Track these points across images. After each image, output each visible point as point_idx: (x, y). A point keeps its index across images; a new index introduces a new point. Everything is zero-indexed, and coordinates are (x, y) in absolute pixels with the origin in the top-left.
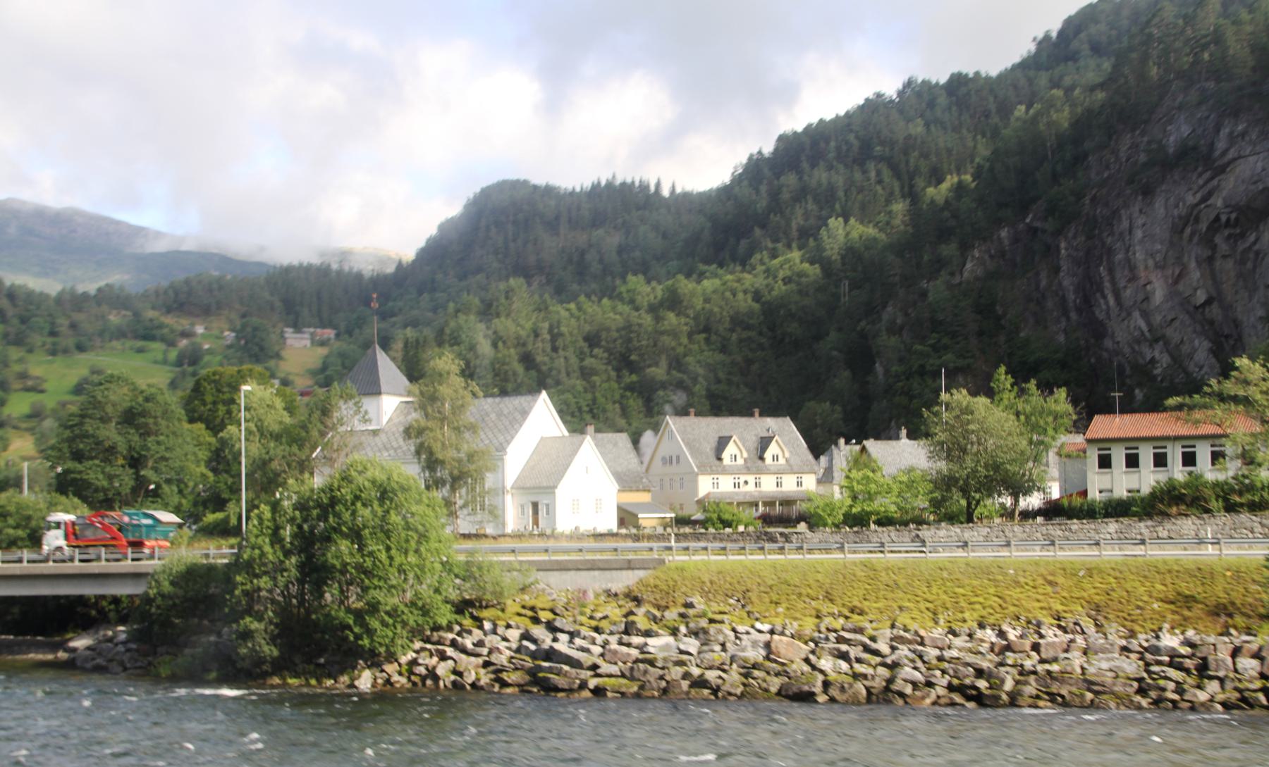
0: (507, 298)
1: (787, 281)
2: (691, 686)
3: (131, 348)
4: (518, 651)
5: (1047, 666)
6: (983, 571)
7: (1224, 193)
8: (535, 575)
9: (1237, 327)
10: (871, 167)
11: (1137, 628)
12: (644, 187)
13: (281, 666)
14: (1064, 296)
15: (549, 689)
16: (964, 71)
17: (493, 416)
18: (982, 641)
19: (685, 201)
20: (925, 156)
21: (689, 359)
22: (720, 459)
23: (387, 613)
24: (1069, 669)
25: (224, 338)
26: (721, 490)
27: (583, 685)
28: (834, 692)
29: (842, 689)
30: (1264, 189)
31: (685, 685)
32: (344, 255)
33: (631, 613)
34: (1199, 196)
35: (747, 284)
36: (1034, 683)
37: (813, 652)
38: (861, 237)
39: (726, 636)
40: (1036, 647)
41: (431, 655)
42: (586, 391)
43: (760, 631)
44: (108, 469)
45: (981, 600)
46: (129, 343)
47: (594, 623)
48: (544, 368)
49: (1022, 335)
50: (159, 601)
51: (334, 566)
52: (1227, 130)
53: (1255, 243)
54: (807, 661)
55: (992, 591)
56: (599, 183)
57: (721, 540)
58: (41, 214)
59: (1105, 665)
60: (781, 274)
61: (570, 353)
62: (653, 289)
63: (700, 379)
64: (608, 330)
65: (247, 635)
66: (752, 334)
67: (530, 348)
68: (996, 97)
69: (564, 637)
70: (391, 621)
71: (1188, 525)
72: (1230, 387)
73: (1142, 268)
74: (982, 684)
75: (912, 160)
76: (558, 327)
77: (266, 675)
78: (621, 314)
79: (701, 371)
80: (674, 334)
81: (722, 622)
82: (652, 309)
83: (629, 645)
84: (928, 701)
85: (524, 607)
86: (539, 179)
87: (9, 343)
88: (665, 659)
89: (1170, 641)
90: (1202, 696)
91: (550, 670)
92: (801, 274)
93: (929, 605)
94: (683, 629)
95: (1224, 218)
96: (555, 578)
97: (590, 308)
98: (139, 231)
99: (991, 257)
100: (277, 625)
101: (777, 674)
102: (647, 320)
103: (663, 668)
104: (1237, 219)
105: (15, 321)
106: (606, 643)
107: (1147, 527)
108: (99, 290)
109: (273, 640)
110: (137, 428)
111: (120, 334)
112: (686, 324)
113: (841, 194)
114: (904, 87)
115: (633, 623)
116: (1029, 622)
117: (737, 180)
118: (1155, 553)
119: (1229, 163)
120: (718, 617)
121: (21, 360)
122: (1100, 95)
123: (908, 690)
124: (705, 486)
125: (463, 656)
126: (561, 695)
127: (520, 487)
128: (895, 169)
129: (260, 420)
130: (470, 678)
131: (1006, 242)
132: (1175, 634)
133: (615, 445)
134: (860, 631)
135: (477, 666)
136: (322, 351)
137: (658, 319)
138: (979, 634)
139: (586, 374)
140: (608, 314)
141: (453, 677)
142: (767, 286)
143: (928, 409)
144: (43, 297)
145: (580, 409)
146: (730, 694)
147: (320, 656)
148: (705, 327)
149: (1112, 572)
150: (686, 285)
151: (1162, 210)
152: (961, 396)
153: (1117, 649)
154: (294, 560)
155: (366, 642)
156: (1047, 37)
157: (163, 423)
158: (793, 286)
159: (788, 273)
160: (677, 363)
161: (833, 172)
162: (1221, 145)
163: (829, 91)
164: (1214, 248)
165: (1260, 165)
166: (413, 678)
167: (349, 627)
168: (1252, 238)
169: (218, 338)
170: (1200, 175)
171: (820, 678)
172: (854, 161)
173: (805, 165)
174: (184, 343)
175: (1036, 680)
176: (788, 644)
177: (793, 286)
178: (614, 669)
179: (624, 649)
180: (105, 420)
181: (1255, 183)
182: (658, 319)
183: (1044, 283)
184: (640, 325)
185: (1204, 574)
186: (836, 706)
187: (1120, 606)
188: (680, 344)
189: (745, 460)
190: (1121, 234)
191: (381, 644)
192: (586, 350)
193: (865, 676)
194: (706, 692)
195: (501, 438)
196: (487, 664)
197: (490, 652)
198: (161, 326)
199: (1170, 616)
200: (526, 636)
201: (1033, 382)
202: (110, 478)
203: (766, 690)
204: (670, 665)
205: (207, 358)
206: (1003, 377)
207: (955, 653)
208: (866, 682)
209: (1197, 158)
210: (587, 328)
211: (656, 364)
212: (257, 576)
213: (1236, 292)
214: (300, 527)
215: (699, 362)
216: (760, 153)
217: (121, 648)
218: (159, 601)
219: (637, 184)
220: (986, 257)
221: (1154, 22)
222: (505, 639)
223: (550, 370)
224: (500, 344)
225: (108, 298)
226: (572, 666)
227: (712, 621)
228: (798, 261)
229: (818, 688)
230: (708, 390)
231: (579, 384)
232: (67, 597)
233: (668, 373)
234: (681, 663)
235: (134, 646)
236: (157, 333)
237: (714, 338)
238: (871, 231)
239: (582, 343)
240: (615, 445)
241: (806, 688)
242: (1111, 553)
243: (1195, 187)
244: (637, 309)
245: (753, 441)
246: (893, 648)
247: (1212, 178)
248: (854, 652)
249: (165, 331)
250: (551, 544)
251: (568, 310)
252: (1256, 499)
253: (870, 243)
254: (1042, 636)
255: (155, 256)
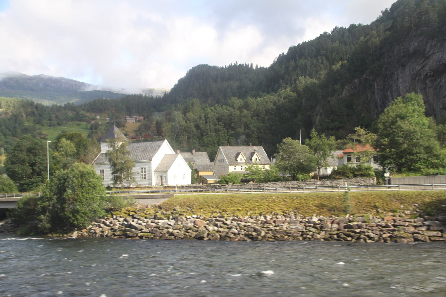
0: (192, 106)
1: (285, 98)
2: (169, 235)
3: (75, 124)
4: (122, 225)
5: (276, 228)
6: (266, 198)
7: (429, 66)
8: (134, 201)
9: (434, 111)
10: (319, 58)
11: (306, 215)
12: (247, 66)
13: (52, 230)
14: (376, 102)
15: (127, 236)
16: (355, 24)
17: (150, 148)
18: (259, 220)
19: (262, 70)
20: (338, 54)
21: (252, 125)
22: (237, 160)
23: (82, 213)
24: (282, 229)
25: (106, 120)
26: (237, 170)
27: (137, 236)
28: (210, 237)
29: (213, 236)
30: (442, 64)
31: (167, 235)
32: (151, 91)
33: (157, 212)
34: (420, 67)
35: (272, 100)
36: (271, 233)
37: (208, 224)
38: (311, 82)
39: (183, 219)
40: (274, 222)
41: (97, 226)
42: (216, 137)
43: (194, 218)
44: (23, 167)
45: (262, 207)
46: (74, 122)
47: (145, 215)
48: (203, 129)
49: (362, 115)
50: (18, 210)
51: (65, 198)
52: (430, 44)
53: (440, 83)
54: (205, 227)
55: (266, 204)
56: (231, 65)
57: (201, 188)
58: (51, 80)
59: (293, 227)
60: (283, 96)
61: (211, 124)
62: (240, 102)
63: (255, 132)
64: (224, 116)
65: (41, 221)
66: (273, 116)
67: (198, 122)
68: (365, 32)
69: (135, 220)
70: (84, 216)
71: (342, 182)
72: (355, 137)
73: (402, 92)
74: (254, 234)
75: (333, 55)
76: (207, 115)
77: (47, 233)
78: (229, 110)
79: (255, 129)
80: (246, 117)
81: (183, 215)
82: (240, 109)
83: (154, 222)
84: (237, 239)
85: (127, 211)
86: (211, 64)
87: (36, 123)
88: (163, 227)
89: (315, 219)
90: (319, 236)
91: (129, 231)
92: (289, 96)
93: (246, 209)
94: (171, 217)
95: (429, 74)
96: (141, 201)
97: (219, 108)
98: (83, 84)
99: (352, 89)
100: (50, 217)
101: (196, 231)
102: (238, 112)
103: (162, 230)
104: (433, 74)
105: (38, 116)
106: (148, 222)
107: (330, 182)
108: (65, 105)
109: (49, 222)
110: (33, 153)
111: (72, 119)
112: (250, 114)
113: (309, 68)
114: (334, 30)
115: (156, 215)
116: (275, 214)
117: (275, 64)
118: (320, 191)
119: (430, 56)
120: (182, 213)
121: (39, 129)
122: (388, 33)
123: (232, 236)
124: (231, 169)
125: (105, 226)
126: (130, 238)
127: (157, 171)
128: (327, 58)
129: (66, 151)
130: (106, 233)
131: (357, 84)
132: (317, 217)
133: (202, 156)
134: (222, 217)
135: (109, 230)
136: (139, 124)
137: (241, 112)
138: (259, 218)
139: (216, 131)
140: (224, 110)
141: (101, 233)
142: (278, 100)
143: (279, 144)
144: (47, 107)
145: (214, 143)
146: (180, 238)
147: (65, 227)
148: (257, 114)
149: (304, 198)
150: (250, 100)
151: (408, 72)
152: (288, 140)
153: (299, 222)
154: (55, 196)
155: (75, 222)
156: (386, 10)
157: (41, 152)
158: (287, 100)
159: (286, 95)
160: (247, 126)
161: (306, 60)
162: (428, 49)
163: (311, 31)
164: (426, 84)
165: (440, 56)
166: (90, 234)
167: (70, 218)
168: (439, 81)
169: (104, 120)
170: (421, 60)
171: (207, 232)
172: (314, 56)
173: (297, 58)
174: (93, 122)
175: (272, 232)
176: (201, 222)
177: (287, 100)
178: (147, 230)
179: (152, 224)
180: (21, 151)
181: (439, 62)
182: (241, 112)
183: (369, 98)
184: (235, 114)
185: (330, 198)
186: (211, 241)
187: (303, 208)
188: (248, 120)
189: (245, 160)
190: (395, 80)
191: (80, 223)
192: (217, 123)
193: (220, 232)
194: (173, 237)
195: (151, 155)
196: (112, 229)
197: (113, 225)
198: (85, 117)
199: (317, 211)
200: (125, 220)
201: (324, 134)
202: (23, 170)
203: (191, 236)
204: (164, 229)
205: (100, 127)
206: (314, 133)
207: (249, 224)
208: (220, 234)
209: (420, 54)
210: (217, 115)
211: (240, 127)
212: (45, 202)
213: (434, 100)
214: (58, 186)
215: (255, 126)
216: (283, 54)
217: (9, 225)
218: (18, 210)
219: (233, 65)
220: (350, 89)
221: (406, 7)
222: (119, 221)
223: (205, 129)
224: (188, 121)
225: (69, 107)
226: (136, 230)
227: (180, 215)
228: (289, 91)
229: (205, 235)
230: (257, 136)
231: (214, 134)
232: (3, 209)
233: (244, 130)
234: (167, 228)
235: (12, 225)
236: (84, 119)
237: (260, 118)
238: (314, 80)
239: (216, 121)
240: (202, 156)
241: (202, 236)
242: (307, 192)
243: (419, 64)
244: (234, 109)
245: (248, 154)
246: (232, 223)
247: (425, 61)
248: (219, 224)
249: (87, 118)
250: (150, 190)
251: (211, 110)
252: (363, 173)
253: (314, 85)
254: (277, 218)
255: (87, 92)
